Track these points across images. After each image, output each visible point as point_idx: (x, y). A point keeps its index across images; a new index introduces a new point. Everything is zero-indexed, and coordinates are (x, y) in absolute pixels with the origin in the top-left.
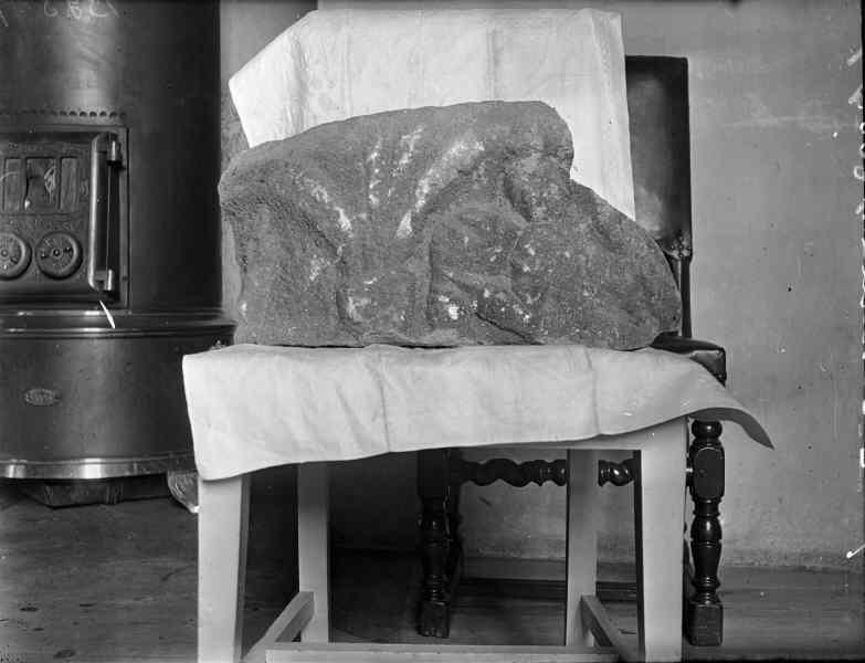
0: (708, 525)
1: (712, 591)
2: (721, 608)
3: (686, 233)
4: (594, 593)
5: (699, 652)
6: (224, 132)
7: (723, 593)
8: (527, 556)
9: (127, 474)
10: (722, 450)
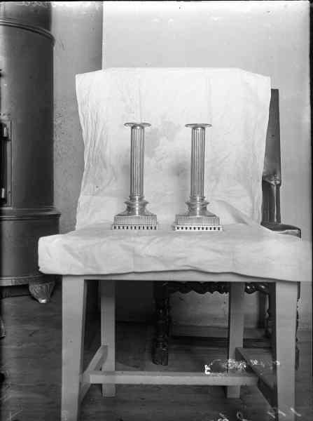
3: (278, 172)
4: (242, 346)
5: (5, 292)
6: (54, 122)
8: (200, 325)
9: (11, 285)
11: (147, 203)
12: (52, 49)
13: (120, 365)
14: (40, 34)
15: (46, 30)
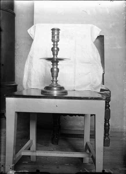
0: (107, 124)
1: (108, 136)
2: (110, 139)
6: (16, 48)
7: (110, 136)
10: (110, 110)
11: (58, 81)
12: (15, 18)
13: (39, 145)
14: (10, 12)
15: (13, 11)
